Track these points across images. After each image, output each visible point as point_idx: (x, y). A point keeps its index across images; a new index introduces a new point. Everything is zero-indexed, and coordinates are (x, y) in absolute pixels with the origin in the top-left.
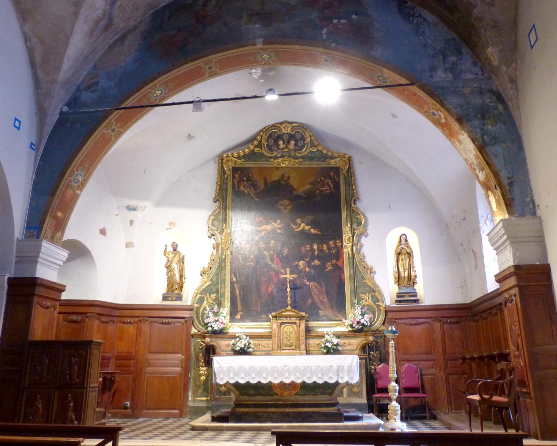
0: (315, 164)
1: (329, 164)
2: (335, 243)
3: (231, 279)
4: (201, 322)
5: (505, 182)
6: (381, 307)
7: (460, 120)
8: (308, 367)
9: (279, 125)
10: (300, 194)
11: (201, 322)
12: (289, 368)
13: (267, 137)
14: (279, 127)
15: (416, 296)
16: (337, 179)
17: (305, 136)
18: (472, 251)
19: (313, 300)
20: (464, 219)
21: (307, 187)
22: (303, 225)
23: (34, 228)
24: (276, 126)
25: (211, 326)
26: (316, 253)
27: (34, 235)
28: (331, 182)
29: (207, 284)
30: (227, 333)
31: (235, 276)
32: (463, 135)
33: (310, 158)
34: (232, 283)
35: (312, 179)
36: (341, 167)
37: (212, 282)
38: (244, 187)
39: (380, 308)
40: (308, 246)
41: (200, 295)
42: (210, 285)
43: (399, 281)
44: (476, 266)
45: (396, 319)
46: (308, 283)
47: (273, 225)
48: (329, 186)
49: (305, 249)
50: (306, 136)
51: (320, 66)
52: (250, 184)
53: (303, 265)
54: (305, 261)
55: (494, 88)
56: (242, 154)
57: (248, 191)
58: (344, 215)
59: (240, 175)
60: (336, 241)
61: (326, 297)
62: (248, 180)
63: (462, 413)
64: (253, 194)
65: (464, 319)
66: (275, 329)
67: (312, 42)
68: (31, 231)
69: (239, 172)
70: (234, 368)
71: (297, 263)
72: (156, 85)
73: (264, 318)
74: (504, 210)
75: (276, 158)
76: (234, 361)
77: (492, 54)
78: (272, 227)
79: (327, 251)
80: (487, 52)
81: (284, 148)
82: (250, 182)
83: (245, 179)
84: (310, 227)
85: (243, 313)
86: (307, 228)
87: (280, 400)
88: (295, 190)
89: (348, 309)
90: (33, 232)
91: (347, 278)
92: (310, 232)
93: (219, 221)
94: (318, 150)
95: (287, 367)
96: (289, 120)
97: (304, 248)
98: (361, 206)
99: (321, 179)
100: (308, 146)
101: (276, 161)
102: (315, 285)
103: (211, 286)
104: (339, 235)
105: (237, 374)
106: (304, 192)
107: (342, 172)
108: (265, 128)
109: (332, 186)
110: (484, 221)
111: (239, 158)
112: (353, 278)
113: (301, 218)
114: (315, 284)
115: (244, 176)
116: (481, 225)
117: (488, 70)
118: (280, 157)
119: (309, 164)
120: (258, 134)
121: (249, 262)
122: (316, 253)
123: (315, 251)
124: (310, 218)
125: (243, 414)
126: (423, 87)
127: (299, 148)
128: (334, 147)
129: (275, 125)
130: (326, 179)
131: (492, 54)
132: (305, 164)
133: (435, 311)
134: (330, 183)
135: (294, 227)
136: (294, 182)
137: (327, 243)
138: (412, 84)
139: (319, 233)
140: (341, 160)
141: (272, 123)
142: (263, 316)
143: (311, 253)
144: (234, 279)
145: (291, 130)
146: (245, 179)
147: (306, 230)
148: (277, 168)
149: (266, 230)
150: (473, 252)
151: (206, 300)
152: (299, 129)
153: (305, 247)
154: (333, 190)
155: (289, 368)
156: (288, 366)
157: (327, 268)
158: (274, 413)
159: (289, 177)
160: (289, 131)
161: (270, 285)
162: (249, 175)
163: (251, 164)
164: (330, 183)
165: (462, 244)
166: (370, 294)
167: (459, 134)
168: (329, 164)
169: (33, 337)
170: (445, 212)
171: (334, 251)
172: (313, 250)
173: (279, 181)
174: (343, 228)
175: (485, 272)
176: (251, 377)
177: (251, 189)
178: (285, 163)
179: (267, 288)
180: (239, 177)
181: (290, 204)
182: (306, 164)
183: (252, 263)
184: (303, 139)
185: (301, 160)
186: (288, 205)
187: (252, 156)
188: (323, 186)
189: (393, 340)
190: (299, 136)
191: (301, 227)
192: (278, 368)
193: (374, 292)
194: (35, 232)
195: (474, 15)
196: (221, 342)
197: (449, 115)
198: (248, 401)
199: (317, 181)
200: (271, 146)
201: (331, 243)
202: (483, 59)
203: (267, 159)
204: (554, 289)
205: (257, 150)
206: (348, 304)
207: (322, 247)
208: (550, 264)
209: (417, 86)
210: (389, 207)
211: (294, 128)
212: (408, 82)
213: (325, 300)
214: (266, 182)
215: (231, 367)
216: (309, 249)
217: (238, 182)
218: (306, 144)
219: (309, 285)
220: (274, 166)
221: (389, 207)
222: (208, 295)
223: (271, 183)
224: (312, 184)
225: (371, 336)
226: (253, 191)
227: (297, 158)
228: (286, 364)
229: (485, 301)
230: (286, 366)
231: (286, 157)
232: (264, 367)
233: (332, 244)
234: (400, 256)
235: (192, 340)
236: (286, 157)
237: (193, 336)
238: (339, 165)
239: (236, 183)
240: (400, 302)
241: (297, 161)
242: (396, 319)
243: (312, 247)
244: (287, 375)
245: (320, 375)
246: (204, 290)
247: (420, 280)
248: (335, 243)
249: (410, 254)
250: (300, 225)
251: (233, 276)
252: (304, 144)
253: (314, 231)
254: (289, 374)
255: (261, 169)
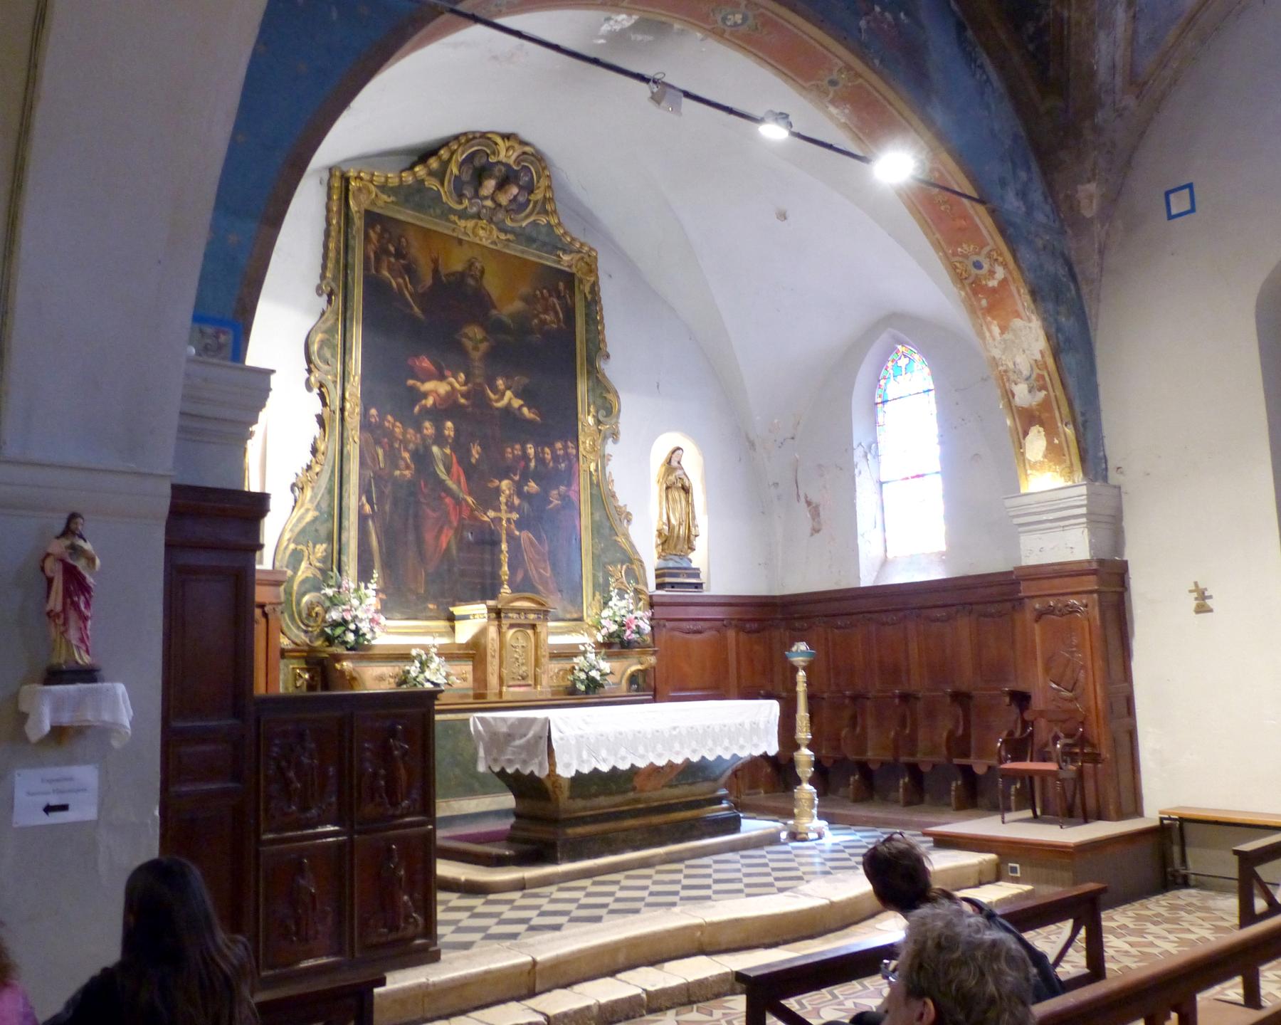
0: (532, 255)
1: (559, 262)
2: (565, 448)
3: (361, 508)
4: (296, 617)
5: (1080, 419)
6: (641, 594)
7: (1034, 293)
8: (708, 727)
9: (499, 140)
10: (505, 319)
11: (296, 617)
12: (680, 732)
13: (464, 156)
14: (496, 144)
15: (697, 575)
16: (569, 301)
17: (538, 182)
18: (803, 499)
19: (526, 572)
20: (793, 438)
21: (518, 305)
22: (509, 394)
23: (219, 323)
24: (489, 139)
25: (356, 632)
26: (533, 464)
27: (220, 347)
28: (559, 304)
29: (309, 517)
30: (370, 647)
31: (369, 501)
32: (1030, 320)
33: (526, 238)
34: (362, 518)
35: (525, 289)
36: (579, 275)
37: (320, 512)
38: (390, 271)
39: (641, 596)
40: (518, 447)
41: (292, 546)
42: (315, 520)
43: (663, 544)
44: (816, 530)
45: (668, 620)
46: (517, 533)
47: (451, 385)
48: (556, 313)
49: (513, 452)
50: (539, 185)
51: (807, 85)
52: (403, 266)
53: (509, 489)
54: (511, 479)
55: (1066, 252)
56: (393, 181)
57: (398, 284)
58: (582, 387)
59: (381, 236)
60: (566, 442)
61: (549, 568)
62: (399, 254)
63: (760, 793)
64: (411, 295)
65: (770, 622)
66: (493, 639)
67: (845, 38)
68: (209, 330)
69: (378, 228)
70: (588, 738)
71: (497, 482)
72: (858, 75)
73: (431, 610)
74: (1072, 464)
75: (463, 215)
76: (587, 723)
77: (1090, 197)
78: (448, 388)
79: (551, 464)
80: (1080, 187)
81: (486, 198)
82: (402, 262)
83: (392, 249)
84: (521, 402)
85: (386, 595)
86: (517, 403)
87: (637, 801)
88: (495, 307)
89: (587, 596)
90: (217, 337)
91: (586, 528)
92: (522, 414)
93: (334, 348)
94: (548, 222)
95: (678, 730)
96: (525, 135)
97: (509, 450)
98: (612, 369)
99: (542, 293)
100: (535, 206)
101: (462, 223)
102: (529, 539)
103: (317, 522)
104: (572, 433)
105: (594, 753)
106: (513, 316)
107: (579, 288)
108: (465, 134)
109: (561, 315)
110: (863, 453)
111: (383, 188)
112: (596, 529)
113: (507, 377)
114: (530, 535)
115: (389, 241)
116: (856, 459)
117: (1062, 216)
118: (472, 217)
119: (523, 252)
120: (445, 143)
121: (400, 470)
122: (533, 464)
123: (530, 460)
124: (521, 380)
125: (584, 839)
126: (993, 212)
127: (517, 207)
128: (572, 228)
129: (489, 136)
130: (550, 296)
131: (1090, 197)
132: (515, 250)
133: (737, 608)
134: (558, 307)
135: (492, 395)
136: (493, 285)
137: (551, 445)
138: (981, 201)
139: (538, 419)
140: (582, 258)
141: (484, 129)
142: (431, 606)
143: (523, 463)
144: (367, 508)
145: (516, 160)
146: (392, 249)
147: (515, 409)
148: (460, 242)
149: (436, 392)
150: (809, 503)
151: (306, 558)
152: (532, 163)
153: (513, 449)
154: (562, 324)
155: (680, 732)
156: (678, 727)
157: (551, 502)
158: (635, 829)
159: (482, 272)
160: (511, 161)
161: (445, 530)
162: (400, 242)
163: (405, 215)
164: (558, 307)
165: (777, 484)
166: (624, 567)
167: (1018, 316)
168: (559, 262)
169: (467, 689)
170: (758, 418)
171: (563, 465)
172: (525, 457)
173: (462, 275)
174: (580, 416)
175: (857, 545)
176: (619, 756)
177: (404, 280)
178: (485, 236)
179: (437, 537)
180: (378, 241)
181: (484, 339)
182: (516, 250)
183: (407, 473)
184: (530, 189)
185: (510, 237)
186: (481, 341)
187: (414, 195)
188: (546, 311)
189: (804, 669)
190: (527, 179)
191: (506, 400)
192: (662, 732)
193: (631, 561)
194: (223, 339)
195: (1096, 120)
196: (365, 669)
197: (1022, 280)
198: (585, 809)
199: (535, 296)
200: (463, 183)
201: (559, 445)
202: (1061, 196)
203: (447, 212)
204: (1130, 601)
205: (432, 184)
206: (587, 585)
207: (543, 452)
208: (1126, 562)
209: (986, 209)
210: (658, 386)
211: (525, 156)
212: (975, 195)
213: (548, 575)
214: (436, 272)
215: (582, 737)
216: (520, 453)
217: (375, 253)
218: (532, 203)
219: (519, 537)
220: (455, 235)
221: (658, 386)
222: (311, 544)
223: (447, 275)
224: (526, 299)
225: (652, 655)
226: (409, 285)
227: (503, 230)
228: (675, 725)
229: (854, 598)
230: (675, 728)
231: (485, 221)
232: (639, 732)
233: (560, 449)
234: (670, 490)
235: (282, 663)
236: (485, 221)
237: (283, 653)
238: (574, 270)
239: (372, 255)
240: (673, 587)
241: (503, 236)
242: (668, 620)
243: (524, 450)
244: (677, 747)
245: (726, 743)
246: (303, 531)
247: (701, 543)
248: (565, 448)
249: (686, 490)
250: (503, 395)
251: (364, 499)
252: (528, 201)
253: (529, 412)
254: (682, 744)
255: (427, 234)
